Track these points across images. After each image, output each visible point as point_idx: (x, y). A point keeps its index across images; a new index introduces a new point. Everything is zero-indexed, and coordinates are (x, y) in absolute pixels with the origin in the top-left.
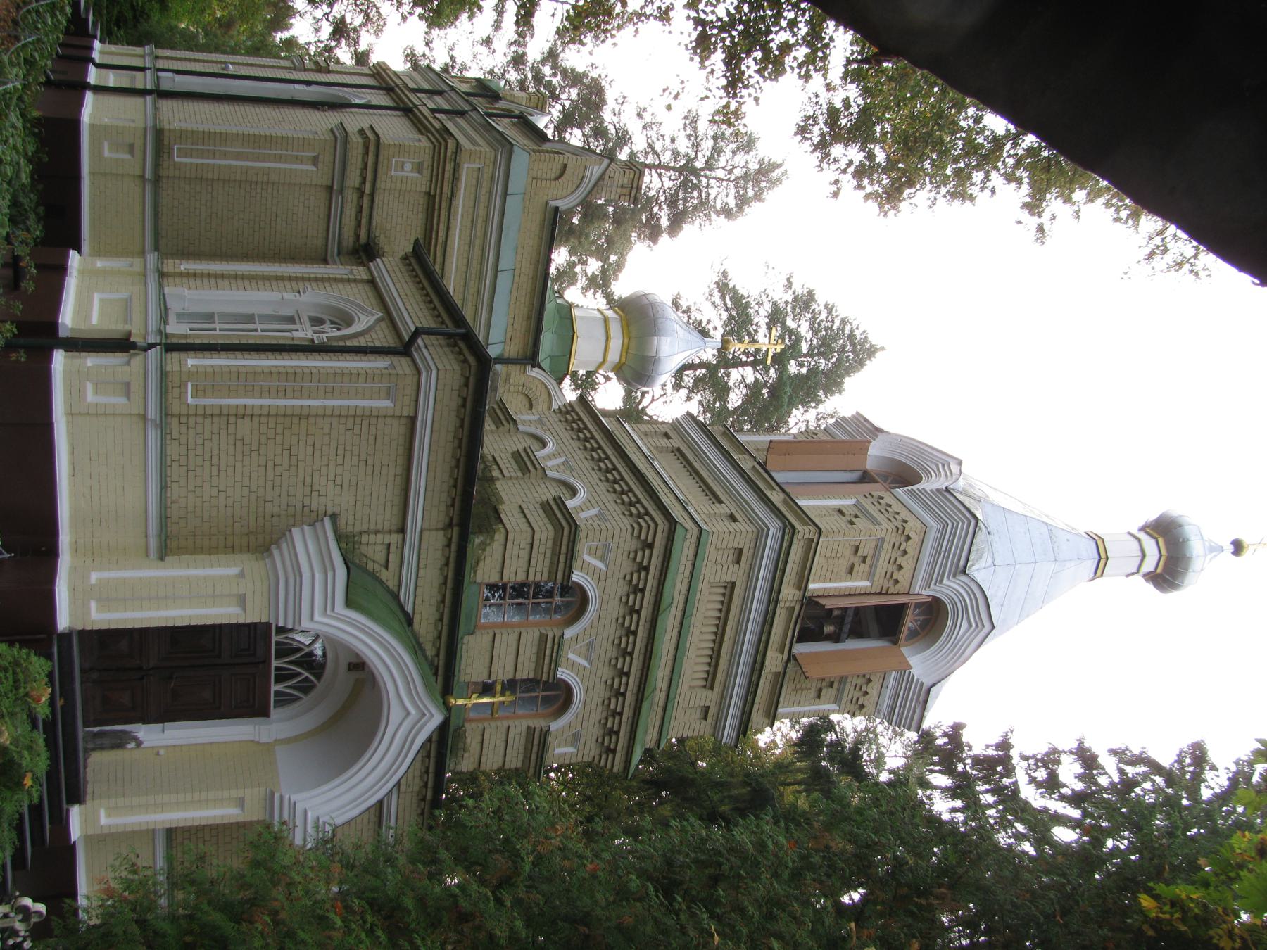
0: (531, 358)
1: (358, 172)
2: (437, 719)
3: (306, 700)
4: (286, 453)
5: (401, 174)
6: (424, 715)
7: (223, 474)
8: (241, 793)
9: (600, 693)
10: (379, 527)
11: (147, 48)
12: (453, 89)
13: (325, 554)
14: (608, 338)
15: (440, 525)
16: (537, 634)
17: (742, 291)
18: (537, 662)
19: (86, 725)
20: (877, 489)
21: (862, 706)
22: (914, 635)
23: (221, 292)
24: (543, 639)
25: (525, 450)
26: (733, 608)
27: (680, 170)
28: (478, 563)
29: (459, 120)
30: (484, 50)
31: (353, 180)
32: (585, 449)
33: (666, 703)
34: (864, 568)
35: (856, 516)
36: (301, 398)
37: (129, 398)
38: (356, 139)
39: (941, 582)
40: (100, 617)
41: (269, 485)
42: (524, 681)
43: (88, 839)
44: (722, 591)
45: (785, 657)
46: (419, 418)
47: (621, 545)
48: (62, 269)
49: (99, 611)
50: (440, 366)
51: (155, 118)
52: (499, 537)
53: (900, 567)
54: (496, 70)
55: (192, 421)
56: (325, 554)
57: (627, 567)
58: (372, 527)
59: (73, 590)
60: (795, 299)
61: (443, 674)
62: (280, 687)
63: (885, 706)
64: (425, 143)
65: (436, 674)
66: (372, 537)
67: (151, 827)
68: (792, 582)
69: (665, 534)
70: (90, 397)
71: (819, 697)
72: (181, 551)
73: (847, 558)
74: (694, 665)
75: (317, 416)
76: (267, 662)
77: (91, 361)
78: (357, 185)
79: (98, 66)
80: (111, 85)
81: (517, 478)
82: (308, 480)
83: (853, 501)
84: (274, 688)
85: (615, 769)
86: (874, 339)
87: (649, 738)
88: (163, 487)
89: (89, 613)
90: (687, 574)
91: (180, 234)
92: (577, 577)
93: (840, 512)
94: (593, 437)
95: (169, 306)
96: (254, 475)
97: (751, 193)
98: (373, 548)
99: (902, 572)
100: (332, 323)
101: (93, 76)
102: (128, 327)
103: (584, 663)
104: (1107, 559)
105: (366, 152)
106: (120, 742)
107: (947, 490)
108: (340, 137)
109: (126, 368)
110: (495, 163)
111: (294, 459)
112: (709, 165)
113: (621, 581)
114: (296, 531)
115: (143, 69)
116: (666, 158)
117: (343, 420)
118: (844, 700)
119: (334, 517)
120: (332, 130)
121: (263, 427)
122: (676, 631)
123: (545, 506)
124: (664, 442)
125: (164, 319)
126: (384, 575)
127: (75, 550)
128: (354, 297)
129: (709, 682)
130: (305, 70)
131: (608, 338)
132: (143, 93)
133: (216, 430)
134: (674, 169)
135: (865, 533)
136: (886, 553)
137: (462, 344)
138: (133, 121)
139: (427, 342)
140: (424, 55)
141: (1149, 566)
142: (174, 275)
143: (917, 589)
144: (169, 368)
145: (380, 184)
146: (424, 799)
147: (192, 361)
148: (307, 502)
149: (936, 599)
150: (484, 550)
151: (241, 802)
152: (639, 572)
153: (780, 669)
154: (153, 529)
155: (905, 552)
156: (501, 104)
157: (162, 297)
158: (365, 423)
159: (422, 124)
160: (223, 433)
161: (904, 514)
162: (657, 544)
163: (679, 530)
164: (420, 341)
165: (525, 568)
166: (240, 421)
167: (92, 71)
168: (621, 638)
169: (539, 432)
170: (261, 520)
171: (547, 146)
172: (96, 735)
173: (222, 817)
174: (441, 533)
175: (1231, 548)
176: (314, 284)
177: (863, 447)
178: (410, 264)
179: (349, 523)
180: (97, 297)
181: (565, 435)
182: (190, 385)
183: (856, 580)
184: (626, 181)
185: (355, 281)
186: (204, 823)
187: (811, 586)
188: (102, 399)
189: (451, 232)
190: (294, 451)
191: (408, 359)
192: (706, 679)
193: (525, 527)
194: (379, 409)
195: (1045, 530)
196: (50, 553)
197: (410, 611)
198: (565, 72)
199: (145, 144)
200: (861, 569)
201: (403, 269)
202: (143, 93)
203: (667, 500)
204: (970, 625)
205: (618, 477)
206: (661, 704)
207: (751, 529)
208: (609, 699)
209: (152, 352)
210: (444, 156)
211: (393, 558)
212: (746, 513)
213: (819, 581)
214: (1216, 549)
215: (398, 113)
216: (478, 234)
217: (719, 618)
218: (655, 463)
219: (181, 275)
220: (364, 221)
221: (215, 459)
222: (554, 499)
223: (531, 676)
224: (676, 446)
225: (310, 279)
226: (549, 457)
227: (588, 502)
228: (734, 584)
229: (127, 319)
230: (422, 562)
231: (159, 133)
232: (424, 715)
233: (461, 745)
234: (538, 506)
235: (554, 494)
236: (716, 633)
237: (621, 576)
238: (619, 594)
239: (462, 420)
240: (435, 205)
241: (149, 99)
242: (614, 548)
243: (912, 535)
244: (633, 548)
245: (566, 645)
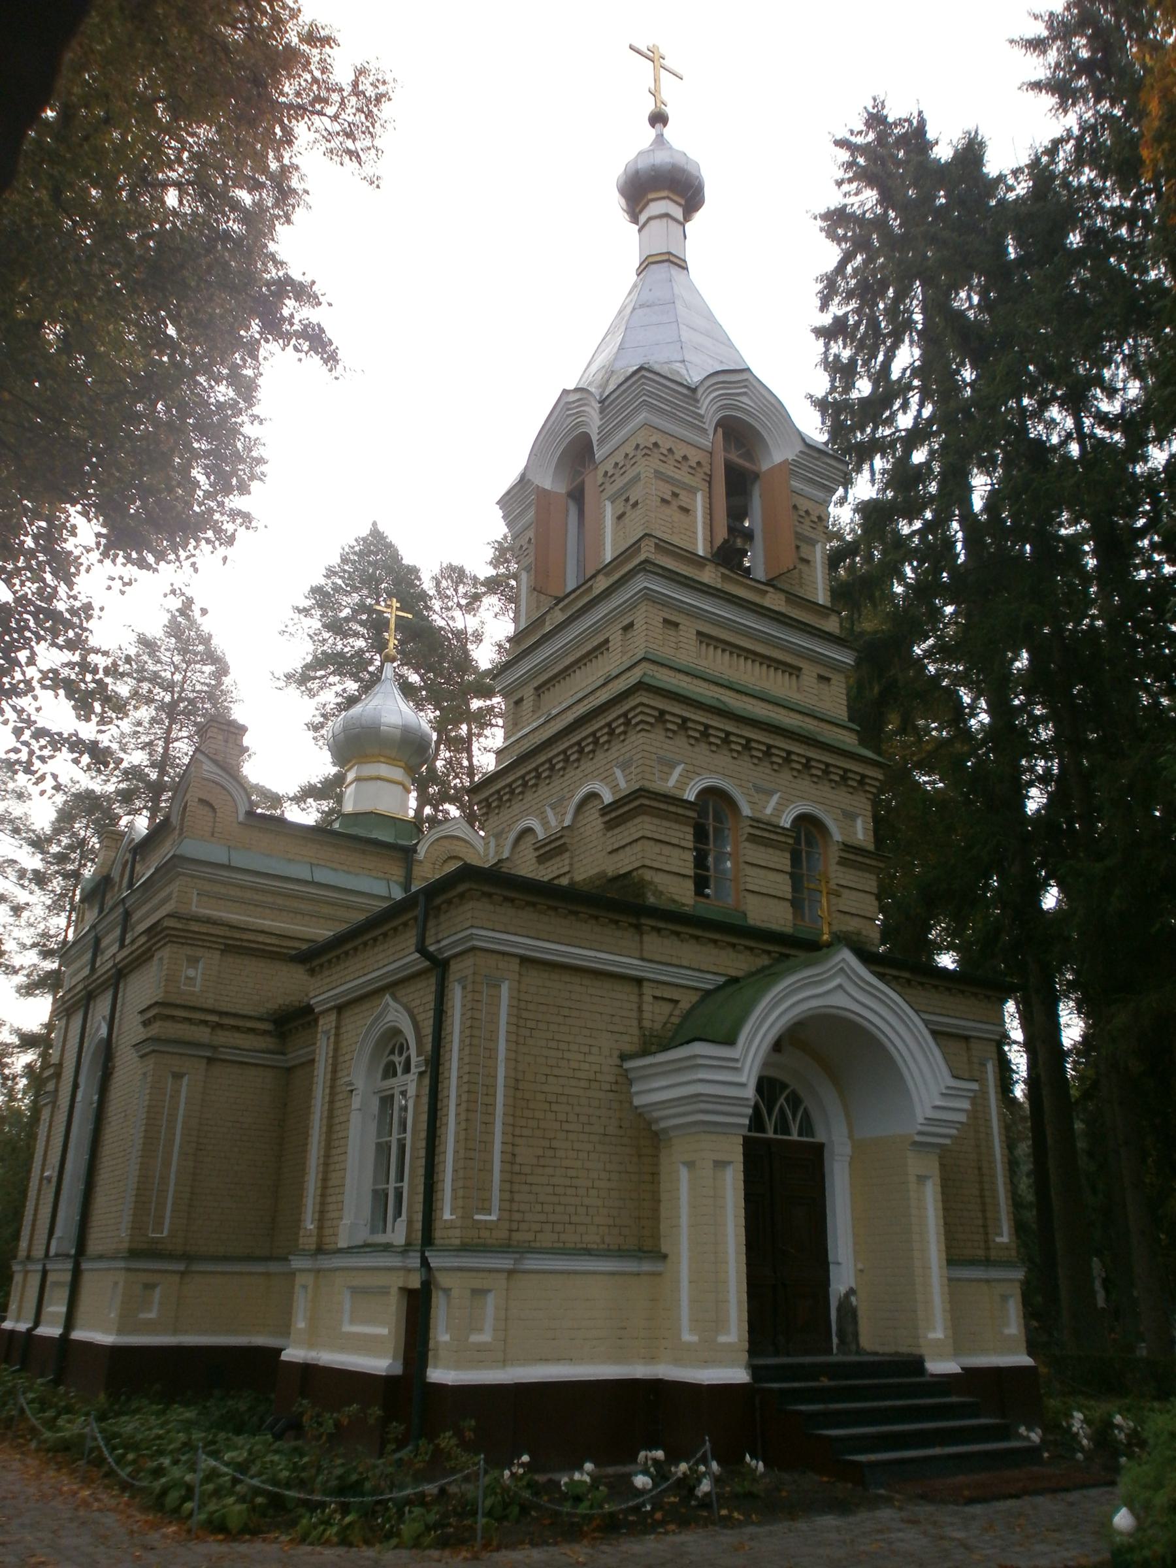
0: (407, 853)
1: (193, 1028)
2: (847, 956)
3: (808, 1102)
4: (554, 1107)
5: (199, 982)
6: (842, 969)
8: (912, 1179)
10: (635, 1006)
11: (16, 1267)
12: (93, 927)
13: (677, 1066)
14: (378, 778)
15: (637, 938)
16: (747, 844)
17: (309, 659)
19: (829, 1351)
20: (591, 482)
22: (749, 455)
23: (348, 1181)
24: (752, 838)
25: (536, 849)
27: (173, 721)
29: (135, 918)
30: (25, 914)
31: (202, 1034)
32: (536, 785)
33: (816, 718)
34: (683, 495)
35: (627, 500)
36: (495, 1086)
37: (489, 1291)
38: (155, 1029)
39: (702, 417)
40: (734, 1331)
42: (792, 866)
44: (704, 645)
47: (658, 744)
48: (308, 1370)
50: (468, 924)
51: (114, 1258)
52: (648, 875)
53: (685, 458)
54: (49, 902)
55: (517, 1216)
56: (677, 1066)
57: (681, 741)
58: (635, 1014)
59: (706, 1363)
60: (321, 606)
61: (795, 947)
62: (795, 1130)
63: (820, 494)
64: (166, 953)
65: (787, 956)
66: (646, 1015)
68: (697, 572)
69: (651, 695)
70: (485, 1337)
72: (656, 1236)
73: (672, 512)
74: (777, 684)
75: (515, 1069)
76: (769, 1142)
77: (441, 1335)
78: (208, 1030)
79: (37, 1324)
80: (64, 1309)
81: (572, 858)
82: (583, 1084)
83: (608, 505)
84: (795, 1137)
85: (881, 777)
86: (365, 532)
87: (848, 740)
88: (588, 1252)
89: (730, 1344)
90: (688, 679)
91: (267, 1229)
92: (690, 795)
93: (620, 517)
94: (523, 777)
95: (361, 1243)
97: (201, 648)
98: (657, 1015)
100: (392, 1052)
101: (50, 1330)
102: (394, 1291)
103: (776, 798)
104: (669, 253)
105: (172, 1018)
106: (848, 1312)
107: (601, 402)
108: (150, 1048)
109: (455, 1293)
110: (193, 876)
111: (563, 1099)
112: (169, 687)
113: (697, 749)
114: (637, 1101)
115: (45, 1273)
116: (158, 730)
117: (521, 1040)
118: (813, 536)
119: (624, 1057)
120: (142, 1057)
121: (526, 1132)
122: (745, 698)
123: (610, 825)
124: (528, 704)
125: (387, 1248)
126: (685, 1005)
127: (652, 1359)
128: (360, 1032)
129: (794, 671)
130: (56, 1090)
131: (378, 778)
132: (77, 1273)
133: (526, 1188)
134: (171, 724)
135: (649, 490)
136: (669, 470)
137: (438, 901)
138: (116, 1283)
139: (432, 940)
140: (28, 976)
141: (678, 213)
142: (320, 1236)
143: (706, 442)
144: (458, 1242)
145: (210, 1004)
146: (909, 981)
147: (446, 1214)
148: (607, 1087)
149: (718, 425)
150: (661, 893)
151: (921, 1179)
152: (687, 729)
153: (782, 596)
154: (630, 1266)
155: (670, 450)
156: (115, 875)
157: (349, 1251)
158: (525, 1014)
159: (144, 953)
160: (530, 1179)
161: (629, 448)
162: (660, 706)
163: (647, 680)
164: (432, 949)
165: (681, 851)
166: (519, 1160)
167: (44, 1331)
168: (752, 756)
169: (512, 836)
171: (175, 820)
172: (842, 1341)
174: (646, 938)
175: (659, 126)
176: (340, 1074)
177: (542, 493)
178: (321, 966)
179: (630, 1042)
180: (348, 1328)
181: (517, 807)
182: (477, 1217)
183: (696, 507)
184: (220, 737)
185: (337, 1028)
186: (942, 1222)
187: (701, 553)
188: (489, 1323)
189: (267, 929)
190: (553, 1098)
191: (452, 963)
192: (791, 674)
193: (637, 847)
194: (511, 998)
195: (639, 311)
196: (657, 1386)
197: (723, 979)
198: (57, 831)
199: (145, 1270)
201: (327, 973)
202: (77, 1273)
203: (603, 696)
204: (745, 394)
205: (496, 796)
206: (815, 723)
207: (643, 607)
208: (812, 775)
209: (434, 1262)
210: (175, 933)
211: (667, 993)
212: (623, 614)
213: (696, 544)
214: (660, 140)
215: (121, 985)
216: (270, 900)
217: (731, 653)
218: (554, 712)
219: (320, 1228)
220: (250, 1024)
221: (559, 1190)
222: (602, 815)
223: (788, 855)
224: (532, 691)
225: (334, 1079)
226: (545, 823)
227: (606, 781)
228: (699, 633)
229: (384, 1291)
230: (675, 961)
231: (134, 1254)
232: (842, 969)
234: (609, 834)
235: (597, 815)
236: (746, 658)
237: (689, 748)
238: (708, 753)
239: (528, 904)
240: (238, 946)
241: (85, 1266)
242: (661, 752)
244: (663, 733)
245: (758, 815)
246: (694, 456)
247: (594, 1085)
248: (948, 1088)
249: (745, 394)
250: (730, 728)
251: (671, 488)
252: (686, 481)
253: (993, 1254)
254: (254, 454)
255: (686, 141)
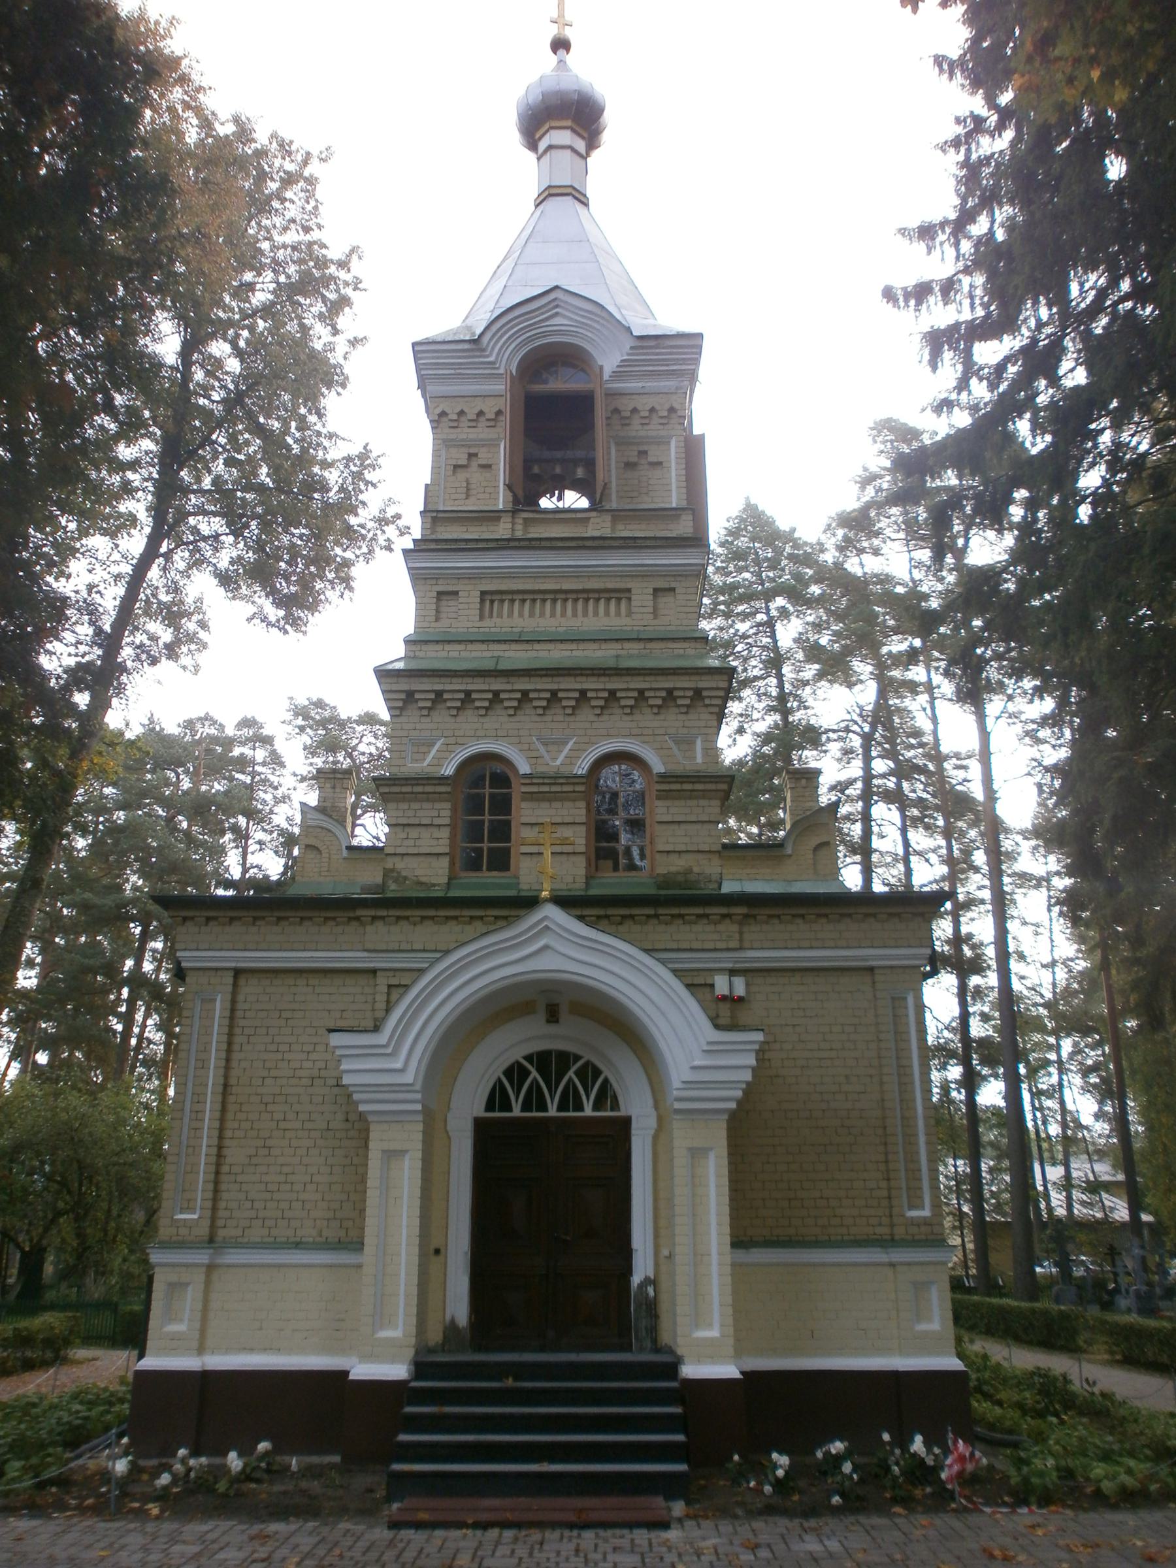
3: (606, 1072)
7: (291, 1178)
9: (470, 721)
18: (550, 800)
21: (672, 410)
26: (514, 587)
28: (422, 883)
37: (188, 1284)
41: (308, 1125)
43: (739, 1352)
45: (594, 514)
46: (233, 965)
47: (411, 726)
49: (710, 1326)
67: (728, 1269)
71: (660, 463)
88: (298, 1245)
89: (712, 1339)
90: (462, 647)
96: (294, 1143)
99: (486, 410)
113: (459, 719)
118: (662, 433)
121: (238, 1134)
150: (405, 878)
160: (240, 1178)
162: (406, 687)
170: (352, 1133)
173: (718, 1176)
175: (561, 52)
200: (484, 456)
230: (404, 946)
232: (547, 927)
233: (680, 878)
243: (438, 411)
246: (490, 410)
247: (317, 1082)
248: (709, 1043)
249: (557, 314)
250: (496, 686)
251: (466, 450)
252: (471, 436)
253: (900, 1232)
254: (361, 497)
255: (587, 70)
